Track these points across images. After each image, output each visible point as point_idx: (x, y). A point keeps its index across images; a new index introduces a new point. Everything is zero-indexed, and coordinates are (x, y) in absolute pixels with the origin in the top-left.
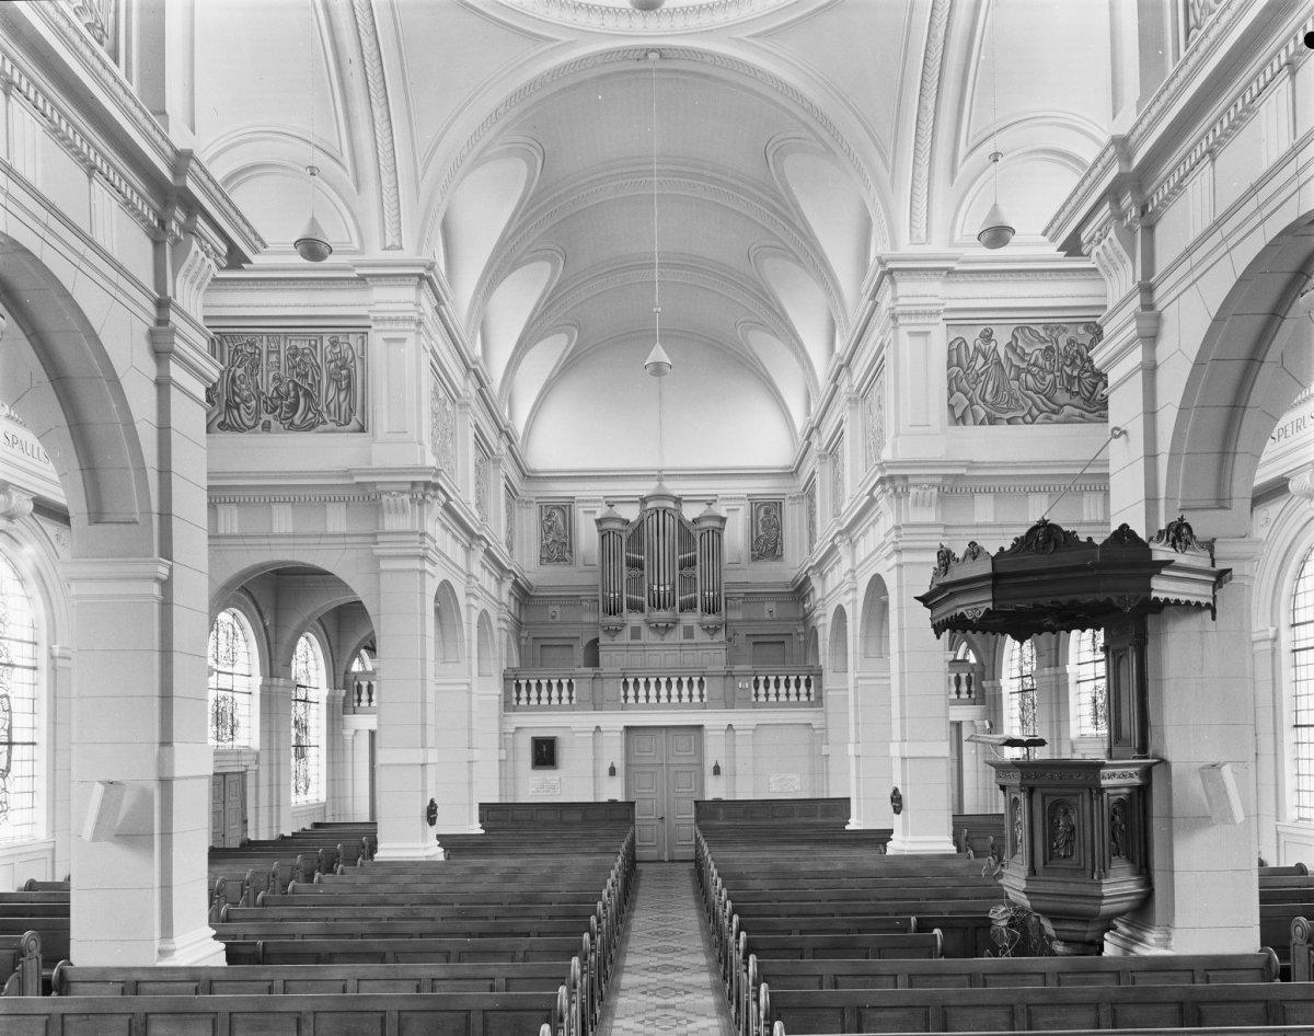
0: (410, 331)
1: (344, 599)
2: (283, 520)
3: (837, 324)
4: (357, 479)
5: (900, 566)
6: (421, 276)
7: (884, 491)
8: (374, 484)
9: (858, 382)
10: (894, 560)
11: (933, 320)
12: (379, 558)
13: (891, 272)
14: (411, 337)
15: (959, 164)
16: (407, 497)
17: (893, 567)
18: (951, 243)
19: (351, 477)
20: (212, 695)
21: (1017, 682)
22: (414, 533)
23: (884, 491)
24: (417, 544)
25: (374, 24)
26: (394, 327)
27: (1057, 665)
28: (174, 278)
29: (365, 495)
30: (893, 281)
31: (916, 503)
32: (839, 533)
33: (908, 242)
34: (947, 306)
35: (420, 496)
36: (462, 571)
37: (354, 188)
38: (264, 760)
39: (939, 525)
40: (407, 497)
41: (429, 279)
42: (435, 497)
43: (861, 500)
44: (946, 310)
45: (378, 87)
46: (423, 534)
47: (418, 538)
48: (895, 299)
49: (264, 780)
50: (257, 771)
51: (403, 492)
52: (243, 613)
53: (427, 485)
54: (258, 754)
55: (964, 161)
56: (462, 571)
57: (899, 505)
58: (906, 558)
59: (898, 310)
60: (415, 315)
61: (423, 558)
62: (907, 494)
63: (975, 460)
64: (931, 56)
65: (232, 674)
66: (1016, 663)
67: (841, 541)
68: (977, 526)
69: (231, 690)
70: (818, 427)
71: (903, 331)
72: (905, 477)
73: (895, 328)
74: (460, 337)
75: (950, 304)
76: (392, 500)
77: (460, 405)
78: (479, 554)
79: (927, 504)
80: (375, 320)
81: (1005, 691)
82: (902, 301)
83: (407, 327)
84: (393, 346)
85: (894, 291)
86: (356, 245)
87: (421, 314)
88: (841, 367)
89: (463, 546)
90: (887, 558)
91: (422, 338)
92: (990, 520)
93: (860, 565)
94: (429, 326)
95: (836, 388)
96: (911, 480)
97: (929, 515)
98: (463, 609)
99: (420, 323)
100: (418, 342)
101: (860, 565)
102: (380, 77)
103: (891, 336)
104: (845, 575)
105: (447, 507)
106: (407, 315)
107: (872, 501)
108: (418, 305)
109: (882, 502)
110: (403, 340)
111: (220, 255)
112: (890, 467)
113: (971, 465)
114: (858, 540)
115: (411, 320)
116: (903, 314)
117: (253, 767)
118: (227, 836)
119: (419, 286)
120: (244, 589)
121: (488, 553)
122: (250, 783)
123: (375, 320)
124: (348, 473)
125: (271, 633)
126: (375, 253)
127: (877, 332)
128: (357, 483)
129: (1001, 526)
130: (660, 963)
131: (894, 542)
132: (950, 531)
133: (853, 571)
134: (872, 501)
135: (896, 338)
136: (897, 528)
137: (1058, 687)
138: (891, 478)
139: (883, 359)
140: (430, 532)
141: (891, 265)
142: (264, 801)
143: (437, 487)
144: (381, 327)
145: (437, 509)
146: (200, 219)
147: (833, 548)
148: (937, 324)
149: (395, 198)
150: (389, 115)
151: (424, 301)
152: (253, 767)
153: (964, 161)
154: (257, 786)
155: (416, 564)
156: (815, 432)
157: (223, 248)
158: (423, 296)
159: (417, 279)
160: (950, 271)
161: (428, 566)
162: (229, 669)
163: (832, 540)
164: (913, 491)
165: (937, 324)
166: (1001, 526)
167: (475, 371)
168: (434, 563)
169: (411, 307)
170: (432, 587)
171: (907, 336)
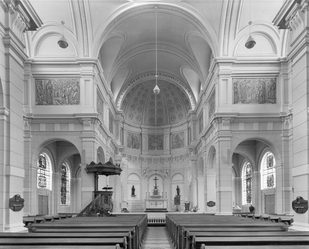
0: (91, 78)
1: (74, 153)
2: (57, 128)
3: (201, 82)
4: (76, 117)
5: (219, 141)
6: (94, 64)
7: (215, 122)
8: (81, 118)
9: (198, 117)
10: (218, 140)
11: (228, 76)
12: (82, 138)
13: (218, 63)
14: (91, 79)
15: (236, 34)
16: (90, 122)
17: (217, 142)
18: (233, 56)
19: (75, 116)
20: (39, 175)
21: (245, 177)
22: (92, 131)
23: (215, 122)
24: (92, 134)
25: (84, 10)
26: (87, 77)
27: (257, 171)
28: (12, 24)
29: (78, 120)
30: (218, 66)
31: (224, 125)
32: (202, 137)
33: (222, 55)
34: (232, 73)
35: (93, 122)
36: (105, 146)
37: (77, 40)
38: (53, 193)
39: (230, 131)
40: (90, 122)
41: (96, 64)
42: (97, 122)
43: (209, 126)
44: (232, 74)
45: (83, 11)
46: (94, 132)
47: (93, 132)
48: (219, 71)
49: (53, 198)
50: (51, 196)
51: (89, 120)
52: (48, 155)
53: (95, 118)
54: (51, 192)
55: (238, 33)
56: (105, 146)
57: (219, 126)
58: (221, 139)
59: (220, 73)
60: (92, 74)
61: (94, 138)
62: (221, 122)
63: (240, 113)
64: (229, 8)
65: (44, 170)
66: (245, 172)
67: (203, 139)
68: (240, 131)
69: (44, 174)
70: (204, 93)
71: (221, 79)
72: (221, 118)
73: (219, 78)
74: (106, 86)
75: (233, 72)
76: (86, 122)
77: (105, 103)
78: (109, 142)
79: (227, 125)
80: (82, 75)
81: (243, 180)
82: (221, 71)
83: (90, 77)
84: (87, 82)
85: (219, 68)
86: (77, 56)
87: (95, 74)
88: (203, 94)
89: (105, 139)
90: (216, 140)
91: (94, 80)
92: (243, 130)
93: (207, 145)
94: (96, 77)
95: (201, 100)
96: (223, 118)
97: (227, 128)
98: (105, 155)
99: (94, 76)
100: (93, 81)
101: (207, 145)
102: (83, 4)
103: (217, 81)
104: (203, 148)
105: (101, 126)
106: (91, 74)
107: (212, 125)
108: (94, 71)
109: (215, 125)
110: (89, 80)
111: (27, 22)
112: (217, 115)
113: (239, 114)
114: (207, 139)
115: (92, 75)
116: (221, 75)
117: (50, 195)
118: (43, 212)
119: (94, 67)
120: (45, 147)
121: (112, 142)
122: (49, 199)
123: (82, 75)
124: (74, 115)
125: (55, 160)
126: (82, 57)
127: (213, 81)
128: (77, 118)
129: (246, 131)
130: (159, 245)
131: (218, 135)
132: (233, 132)
133: (205, 146)
134: (212, 125)
135: (219, 81)
136: (218, 131)
137: (258, 176)
138: (217, 118)
139: (215, 88)
140: (96, 132)
141: (218, 61)
142: (53, 204)
143: (98, 119)
144: (84, 77)
145: (98, 126)
146: (19, 6)
147: (201, 141)
148: (230, 77)
149: (87, 43)
150: (84, 6)
151: (95, 70)
152: (50, 195)
153: (238, 33)
154: (51, 200)
155: (92, 140)
156: (204, 95)
157: (29, 20)
158: (95, 69)
159: (93, 64)
160: (233, 63)
161: (95, 140)
162: (44, 169)
163: (200, 140)
164: (223, 121)
165: (230, 77)
166: (246, 131)
167: (109, 94)
168: (97, 140)
169: (92, 71)
170: (97, 147)
171: (221, 80)
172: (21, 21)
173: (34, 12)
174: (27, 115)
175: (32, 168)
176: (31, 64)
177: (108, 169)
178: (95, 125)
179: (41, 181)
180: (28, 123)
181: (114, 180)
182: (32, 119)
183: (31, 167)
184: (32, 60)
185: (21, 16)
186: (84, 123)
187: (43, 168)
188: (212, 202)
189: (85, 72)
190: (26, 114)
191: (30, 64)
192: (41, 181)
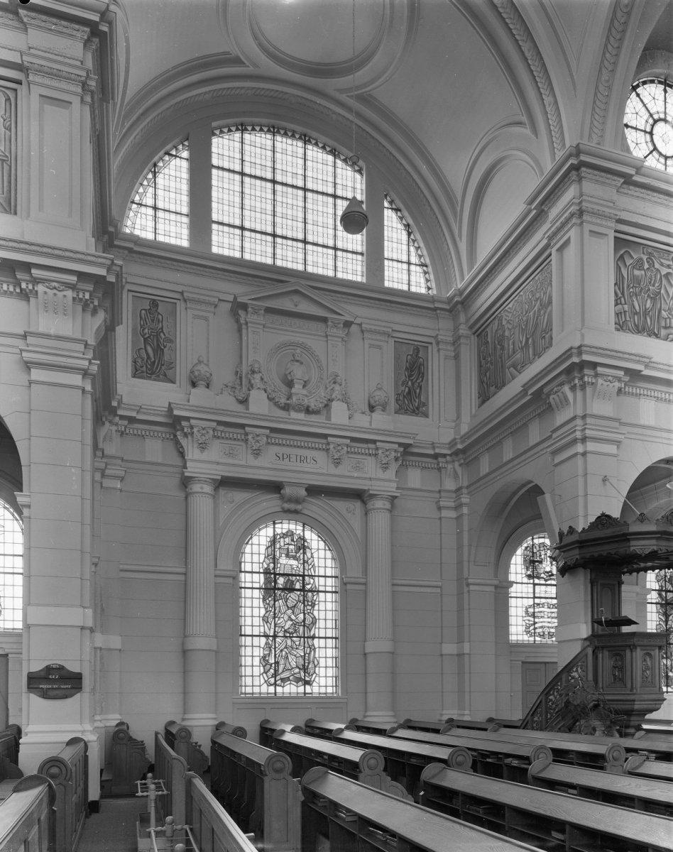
76: (555, 396)
159: (574, 173)
172: (55, 294)
173: (71, 255)
174: (450, 448)
175: (472, 588)
176: (462, 303)
177: (644, 539)
178: (589, 390)
179: (536, 620)
180: (460, 465)
181: (492, 589)
182: (464, 451)
183: (468, 585)
184: (458, 293)
185: (47, 287)
186: (553, 403)
187: (546, 580)
188: (62, 668)
189: (209, 293)
190: (447, 446)
191: (459, 306)
192: (536, 620)
